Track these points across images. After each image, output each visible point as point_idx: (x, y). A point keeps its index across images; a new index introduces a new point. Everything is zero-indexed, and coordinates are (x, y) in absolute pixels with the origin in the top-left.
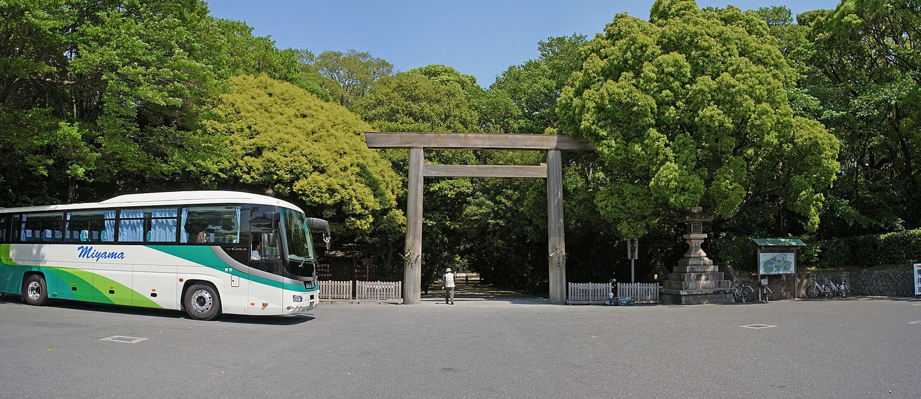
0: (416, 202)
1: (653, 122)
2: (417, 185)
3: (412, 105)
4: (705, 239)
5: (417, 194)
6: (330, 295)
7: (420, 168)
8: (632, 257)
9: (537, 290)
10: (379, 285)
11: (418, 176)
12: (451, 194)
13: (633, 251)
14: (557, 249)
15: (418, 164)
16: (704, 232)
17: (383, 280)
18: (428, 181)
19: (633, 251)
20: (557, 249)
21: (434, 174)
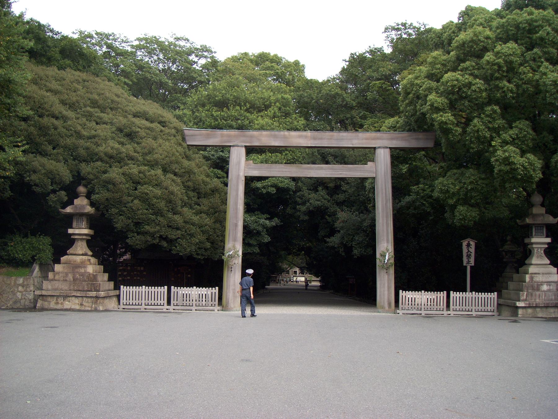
0: (236, 204)
1: (522, 69)
2: (238, 185)
3: (63, 110)
4: (548, 244)
5: (237, 195)
6: (143, 302)
7: (240, 167)
8: (468, 262)
9: (366, 296)
10: (195, 292)
11: (239, 175)
12: (273, 190)
13: (469, 256)
14: (385, 247)
15: (239, 163)
16: (547, 237)
17: (198, 286)
18: (249, 180)
19: (469, 256)
20: (385, 247)
21: (255, 173)
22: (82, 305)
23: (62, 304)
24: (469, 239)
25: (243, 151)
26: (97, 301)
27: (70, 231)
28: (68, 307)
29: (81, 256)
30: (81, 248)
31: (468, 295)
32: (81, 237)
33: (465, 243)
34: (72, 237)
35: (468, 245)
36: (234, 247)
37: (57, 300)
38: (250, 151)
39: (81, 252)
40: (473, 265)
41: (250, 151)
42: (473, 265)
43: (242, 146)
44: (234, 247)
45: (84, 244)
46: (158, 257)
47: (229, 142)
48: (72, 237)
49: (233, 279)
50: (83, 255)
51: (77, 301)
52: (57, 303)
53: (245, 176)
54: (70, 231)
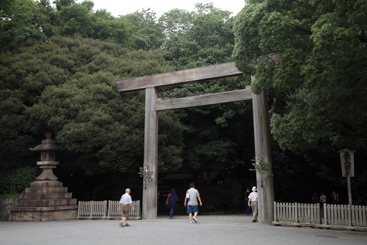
7: (153, 104)
8: (347, 173)
13: (348, 167)
22: (33, 217)
23: (23, 217)
24: (346, 150)
25: (154, 90)
26: (42, 214)
27: (39, 163)
28: (26, 219)
29: (43, 181)
30: (47, 174)
31: (350, 207)
32: (47, 167)
33: (342, 155)
34: (40, 167)
35: (347, 156)
36: (150, 167)
37: (20, 215)
38: (159, 90)
39: (43, 178)
40: (353, 176)
41: (159, 90)
42: (353, 176)
43: (152, 88)
44: (150, 167)
45: (51, 171)
46: (96, 178)
47: (145, 85)
48: (40, 167)
49: (150, 192)
50: (44, 180)
51: (31, 215)
52: (20, 217)
53: (252, 100)
54: (39, 163)
